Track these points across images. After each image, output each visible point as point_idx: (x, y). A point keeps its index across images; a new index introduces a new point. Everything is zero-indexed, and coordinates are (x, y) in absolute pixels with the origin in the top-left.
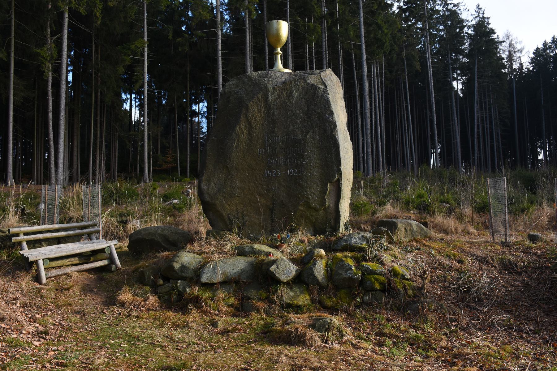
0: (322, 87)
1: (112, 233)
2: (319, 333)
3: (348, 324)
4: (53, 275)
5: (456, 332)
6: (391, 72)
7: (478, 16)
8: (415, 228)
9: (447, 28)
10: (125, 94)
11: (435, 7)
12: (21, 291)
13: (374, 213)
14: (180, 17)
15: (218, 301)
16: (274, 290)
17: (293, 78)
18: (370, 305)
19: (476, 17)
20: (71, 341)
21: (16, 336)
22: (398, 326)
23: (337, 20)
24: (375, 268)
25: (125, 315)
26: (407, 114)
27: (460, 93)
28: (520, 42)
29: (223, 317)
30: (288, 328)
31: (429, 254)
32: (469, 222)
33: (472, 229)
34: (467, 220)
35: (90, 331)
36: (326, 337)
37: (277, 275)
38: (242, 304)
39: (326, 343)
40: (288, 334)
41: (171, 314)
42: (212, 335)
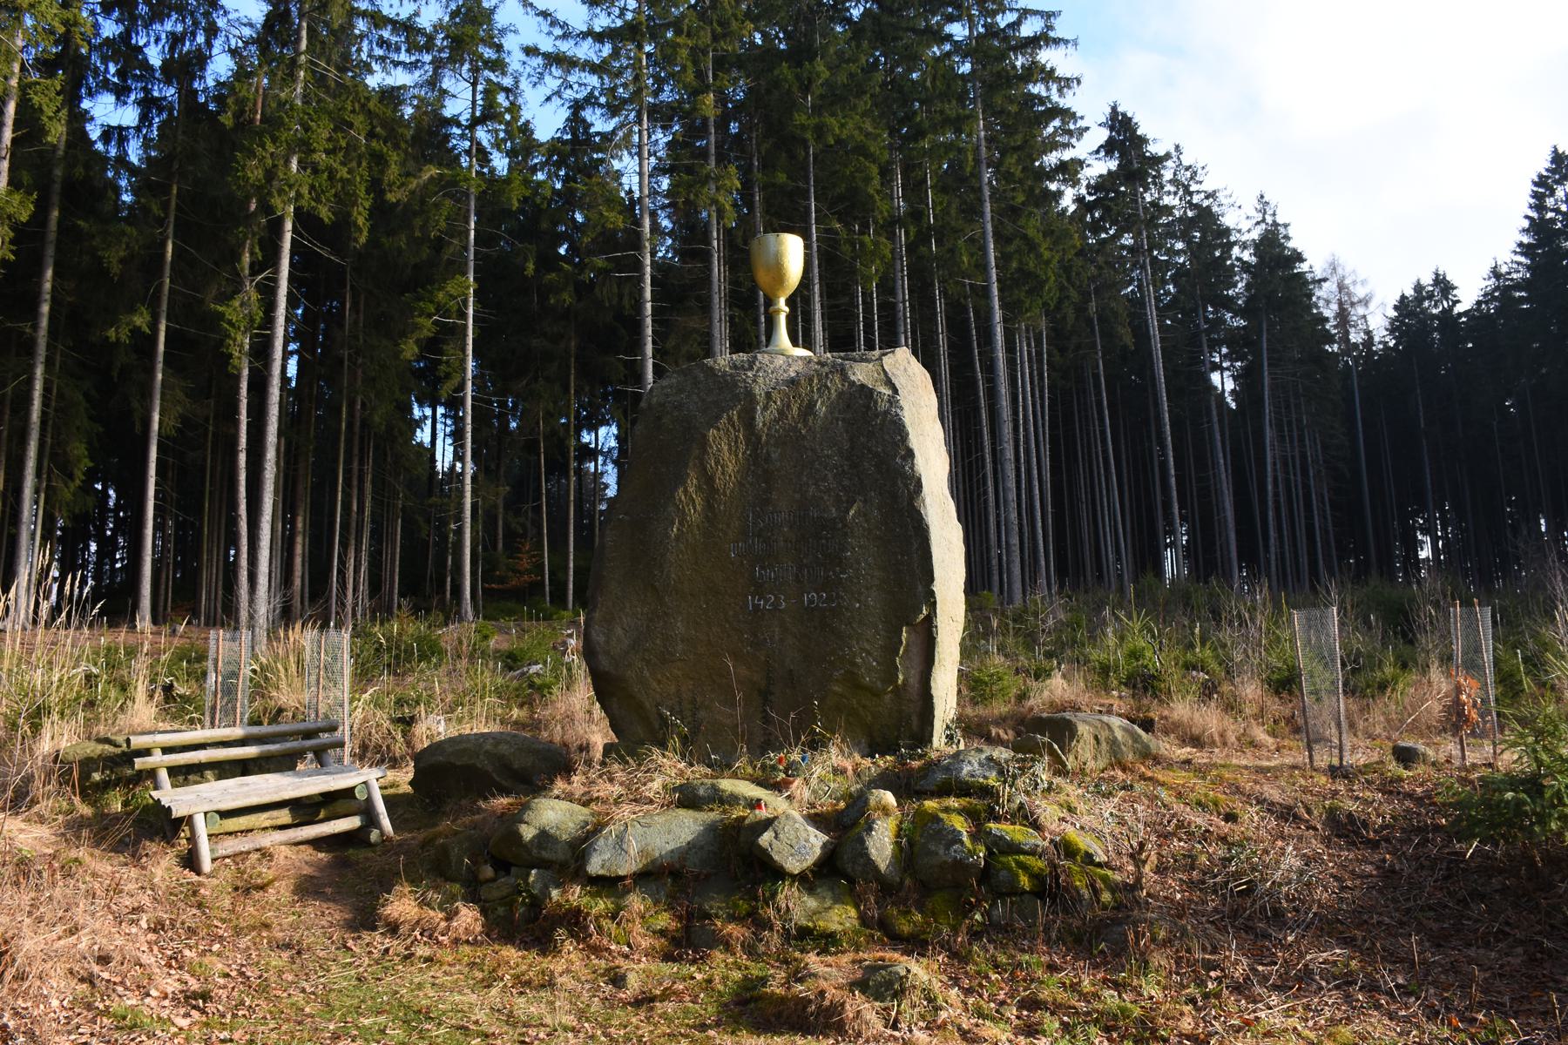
0: (887, 391)
1: (378, 748)
2: (877, 1004)
3: (950, 978)
4: (229, 851)
5: (1218, 995)
6: (1062, 350)
7: (1264, 220)
8: (1119, 734)
9: (1193, 250)
10: (421, 406)
11: (1160, 198)
12: (153, 890)
13: (1022, 697)
14: (556, 224)
15: (628, 921)
16: (767, 894)
17: (816, 370)
18: (1007, 931)
19: (1258, 223)
20: (264, 1018)
21: (134, 1002)
22: (1076, 984)
23: (929, 227)
24: (1019, 837)
25: (398, 955)
26: (1105, 451)
27: (1229, 399)
28: (1364, 282)
29: (640, 961)
30: (801, 992)
31: (1153, 798)
32: (1256, 717)
33: (1260, 734)
34: (1248, 711)
35: (313, 993)
36: (893, 1014)
37: (776, 857)
38: (687, 929)
39: (895, 1027)
40: (800, 1007)
41: (511, 953)
42: (612, 1007)
